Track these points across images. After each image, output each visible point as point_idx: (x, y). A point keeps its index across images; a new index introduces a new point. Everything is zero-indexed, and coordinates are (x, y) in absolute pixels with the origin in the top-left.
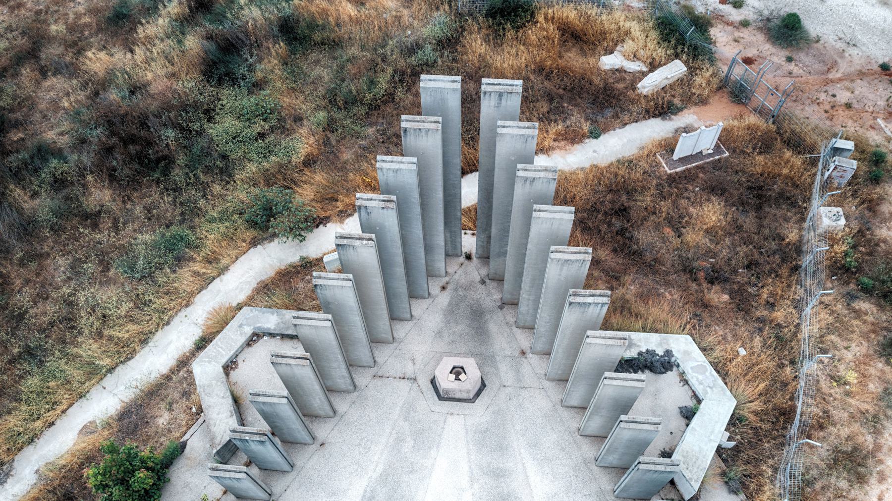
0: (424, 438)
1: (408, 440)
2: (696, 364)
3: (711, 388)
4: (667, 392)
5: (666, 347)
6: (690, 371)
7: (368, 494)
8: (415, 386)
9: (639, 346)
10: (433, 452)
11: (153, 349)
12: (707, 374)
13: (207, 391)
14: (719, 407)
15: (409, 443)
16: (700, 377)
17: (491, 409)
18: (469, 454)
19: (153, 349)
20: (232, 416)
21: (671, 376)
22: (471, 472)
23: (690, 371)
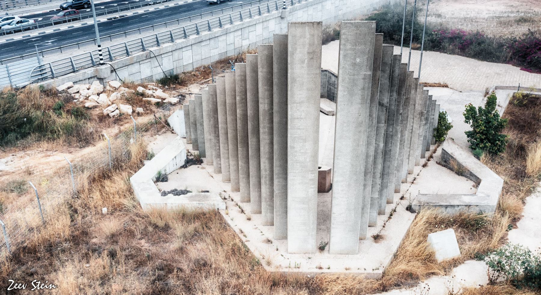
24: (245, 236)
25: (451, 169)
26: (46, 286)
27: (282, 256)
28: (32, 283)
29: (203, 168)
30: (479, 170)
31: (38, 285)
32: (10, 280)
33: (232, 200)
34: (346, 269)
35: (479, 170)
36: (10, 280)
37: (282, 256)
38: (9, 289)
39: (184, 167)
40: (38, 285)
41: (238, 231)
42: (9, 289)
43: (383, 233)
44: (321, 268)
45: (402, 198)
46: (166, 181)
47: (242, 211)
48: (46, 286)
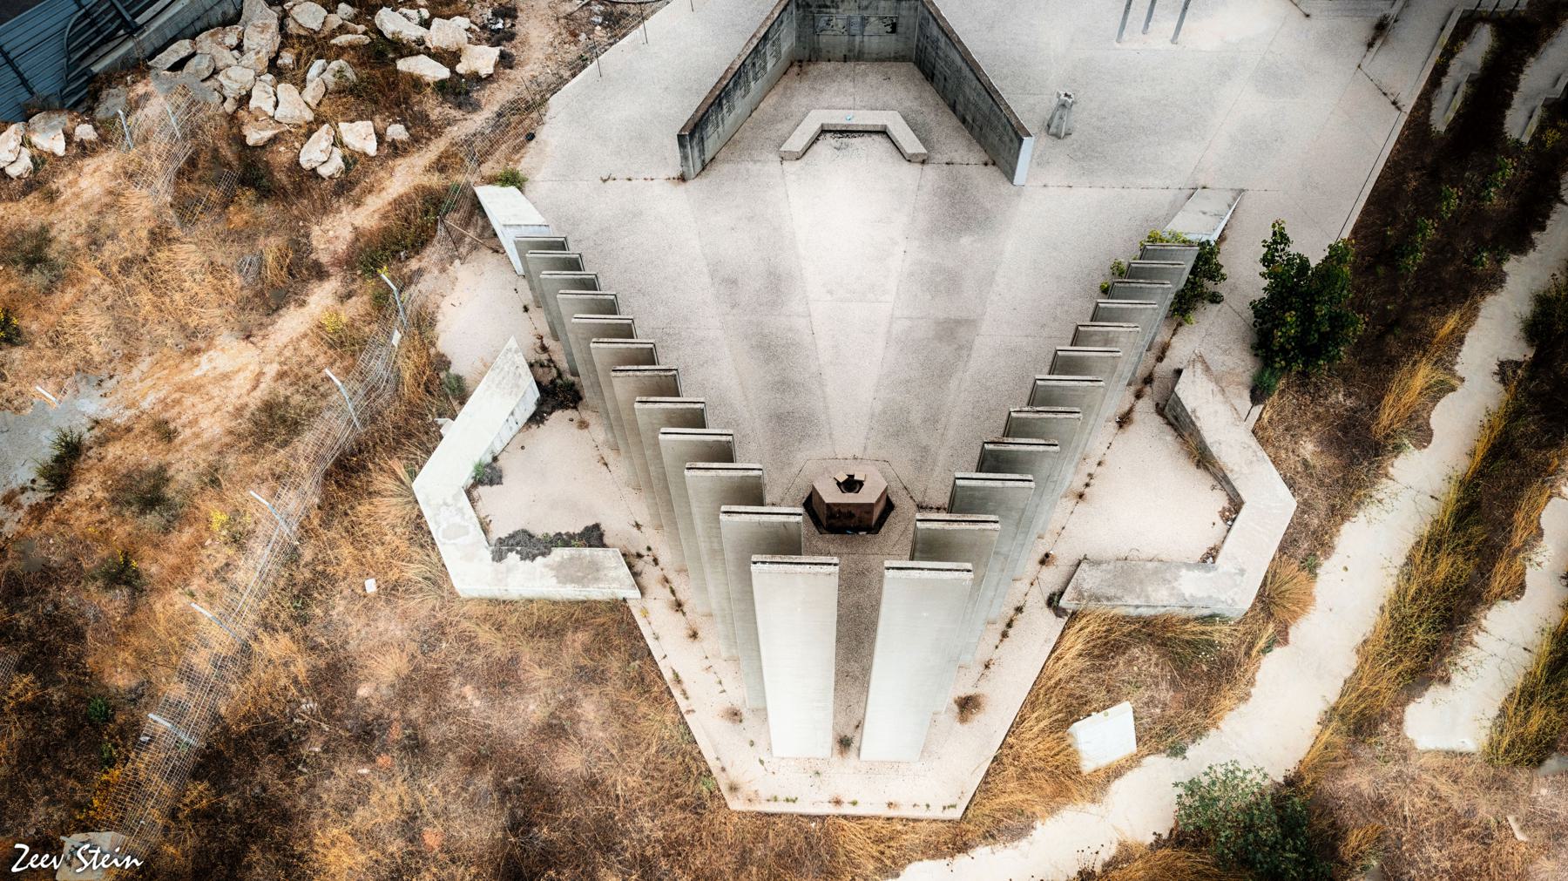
0: (895, 426)
1: (918, 422)
2: (459, 541)
3: (446, 504)
4: (510, 508)
5: (502, 566)
6: (471, 528)
7: (964, 353)
8: (919, 499)
9: (546, 566)
10: (878, 407)
11: (1386, 563)
12: (444, 525)
13: (1250, 452)
14: (439, 480)
15: (916, 417)
16: (458, 519)
17: (795, 470)
18: (827, 408)
19: (1386, 563)
20: (1194, 411)
21: (501, 530)
22: (822, 385)
23: (471, 528)
24: (684, 693)
25: (944, 97)
26: (115, 861)
27: (762, 762)
28: (79, 854)
29: (583, 425)
30: (1246, 470)
31: (95, 858)
32: (18, 846)
33: (656, 561)
34: (890, 805)
35: (1246, 470)
36: (18, 846)
37: (762, 762)
38: (15, 869)
39: (537, 418)
40: (95, 858)
41: (668, 676)
42: (15, 869)
43: (984, 689)
44: (838, 802)
45: (1045, 560)
46: (500, 483)
47: (679, 606)
48: (115, 861)
